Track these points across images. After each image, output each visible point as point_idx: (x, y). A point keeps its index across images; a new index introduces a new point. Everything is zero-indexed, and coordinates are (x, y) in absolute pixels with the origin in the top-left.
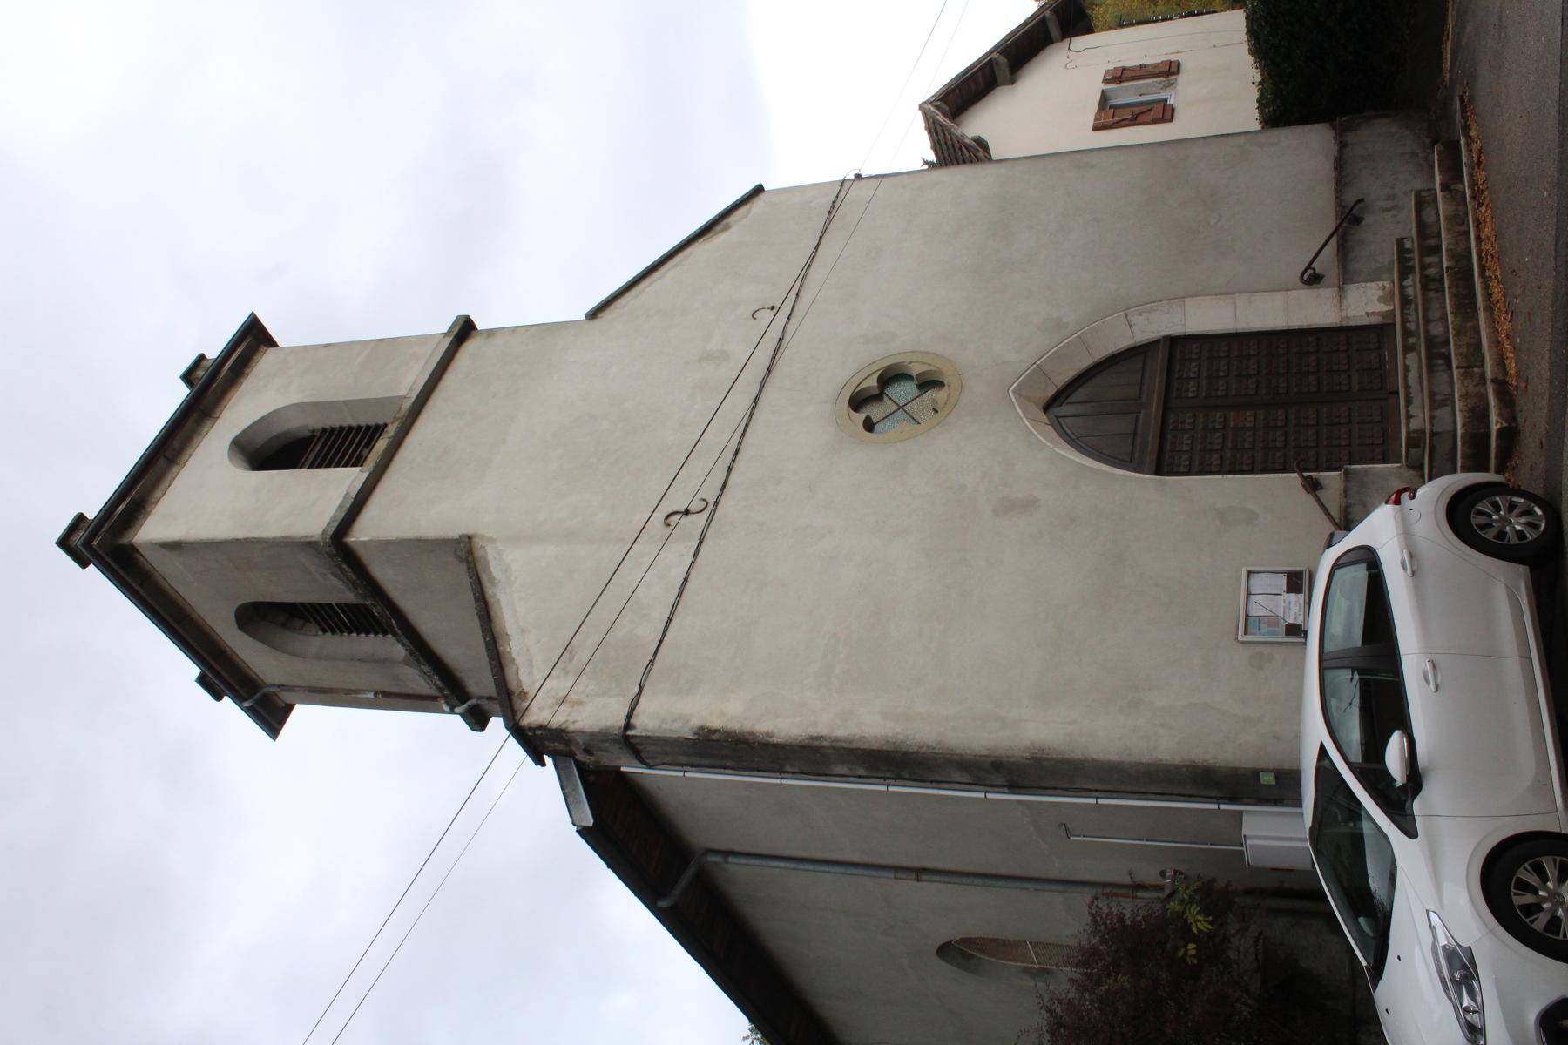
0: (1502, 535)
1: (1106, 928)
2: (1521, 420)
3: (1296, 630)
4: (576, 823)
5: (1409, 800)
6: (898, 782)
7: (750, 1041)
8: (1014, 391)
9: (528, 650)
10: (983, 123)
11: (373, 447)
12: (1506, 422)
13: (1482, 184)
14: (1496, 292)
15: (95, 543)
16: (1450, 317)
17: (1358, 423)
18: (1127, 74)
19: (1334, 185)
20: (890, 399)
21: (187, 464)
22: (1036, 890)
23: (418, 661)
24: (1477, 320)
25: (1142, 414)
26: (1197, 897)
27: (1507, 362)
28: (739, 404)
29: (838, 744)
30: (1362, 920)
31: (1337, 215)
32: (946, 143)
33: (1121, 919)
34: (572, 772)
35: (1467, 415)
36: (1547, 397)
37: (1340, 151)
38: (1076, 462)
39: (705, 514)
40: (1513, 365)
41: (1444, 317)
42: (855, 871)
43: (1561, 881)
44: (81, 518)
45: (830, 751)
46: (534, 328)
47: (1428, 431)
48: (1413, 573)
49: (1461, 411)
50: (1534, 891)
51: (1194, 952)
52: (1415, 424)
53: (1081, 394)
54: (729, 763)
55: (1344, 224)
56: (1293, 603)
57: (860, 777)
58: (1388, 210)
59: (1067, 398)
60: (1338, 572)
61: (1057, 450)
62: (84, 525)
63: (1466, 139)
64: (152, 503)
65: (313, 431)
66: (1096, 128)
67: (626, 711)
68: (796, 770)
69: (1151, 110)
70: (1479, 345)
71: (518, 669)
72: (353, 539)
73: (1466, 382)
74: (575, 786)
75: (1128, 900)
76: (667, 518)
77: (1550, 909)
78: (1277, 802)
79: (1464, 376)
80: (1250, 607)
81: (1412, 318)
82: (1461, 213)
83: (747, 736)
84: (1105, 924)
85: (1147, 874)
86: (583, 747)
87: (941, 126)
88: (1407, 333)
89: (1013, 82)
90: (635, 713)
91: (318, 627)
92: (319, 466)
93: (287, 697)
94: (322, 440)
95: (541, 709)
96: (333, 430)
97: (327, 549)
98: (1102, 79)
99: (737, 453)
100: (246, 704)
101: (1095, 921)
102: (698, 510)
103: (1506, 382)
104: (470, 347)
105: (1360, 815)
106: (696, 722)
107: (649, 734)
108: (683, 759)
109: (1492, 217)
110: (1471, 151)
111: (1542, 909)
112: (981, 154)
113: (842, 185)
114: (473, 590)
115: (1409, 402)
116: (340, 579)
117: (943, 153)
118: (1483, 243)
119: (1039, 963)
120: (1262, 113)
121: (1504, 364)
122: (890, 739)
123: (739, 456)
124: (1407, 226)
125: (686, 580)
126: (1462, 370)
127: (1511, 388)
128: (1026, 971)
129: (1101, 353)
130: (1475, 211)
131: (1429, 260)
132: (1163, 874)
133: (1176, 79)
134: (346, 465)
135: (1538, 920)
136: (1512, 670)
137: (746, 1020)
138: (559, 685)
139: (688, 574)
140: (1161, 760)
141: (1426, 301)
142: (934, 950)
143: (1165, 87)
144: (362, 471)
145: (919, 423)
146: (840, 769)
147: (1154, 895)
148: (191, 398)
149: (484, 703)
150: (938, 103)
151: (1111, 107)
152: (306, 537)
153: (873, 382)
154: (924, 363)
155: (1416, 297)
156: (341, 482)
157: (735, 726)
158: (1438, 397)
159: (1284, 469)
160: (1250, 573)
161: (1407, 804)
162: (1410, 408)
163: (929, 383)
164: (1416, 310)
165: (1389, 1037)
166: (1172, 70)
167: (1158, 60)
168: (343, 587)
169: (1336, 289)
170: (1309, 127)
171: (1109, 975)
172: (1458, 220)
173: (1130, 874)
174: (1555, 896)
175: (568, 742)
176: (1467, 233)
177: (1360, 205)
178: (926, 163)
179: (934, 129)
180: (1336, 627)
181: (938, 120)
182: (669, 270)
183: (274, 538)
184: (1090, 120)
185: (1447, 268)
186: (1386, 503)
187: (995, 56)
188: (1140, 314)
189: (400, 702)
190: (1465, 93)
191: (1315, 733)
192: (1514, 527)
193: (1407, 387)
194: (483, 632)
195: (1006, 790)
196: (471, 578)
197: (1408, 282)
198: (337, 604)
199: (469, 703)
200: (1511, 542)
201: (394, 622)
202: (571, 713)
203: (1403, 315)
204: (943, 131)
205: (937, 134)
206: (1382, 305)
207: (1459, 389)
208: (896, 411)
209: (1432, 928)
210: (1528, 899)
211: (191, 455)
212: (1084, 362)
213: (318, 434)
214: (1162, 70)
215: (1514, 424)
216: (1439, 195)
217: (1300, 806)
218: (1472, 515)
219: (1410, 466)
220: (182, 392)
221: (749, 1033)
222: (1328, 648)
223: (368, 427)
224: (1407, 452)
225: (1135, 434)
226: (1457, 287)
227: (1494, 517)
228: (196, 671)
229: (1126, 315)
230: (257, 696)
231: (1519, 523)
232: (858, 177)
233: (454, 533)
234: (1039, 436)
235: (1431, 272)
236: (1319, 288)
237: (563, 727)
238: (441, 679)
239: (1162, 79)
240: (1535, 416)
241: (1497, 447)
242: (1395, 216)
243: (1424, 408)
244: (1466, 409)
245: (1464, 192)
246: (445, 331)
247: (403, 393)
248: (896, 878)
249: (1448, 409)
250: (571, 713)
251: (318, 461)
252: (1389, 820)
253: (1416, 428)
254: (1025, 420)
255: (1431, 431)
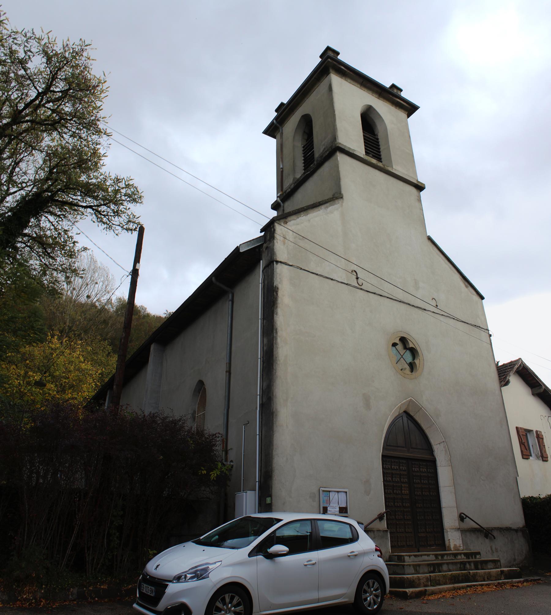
0: (366, 592)
1: (211, 440)
2: (411, 601)
3: (325, 511)
4: (241, 246)
5: (263, 554)
6: (262, 362)
7: (166, 312)
8: (411, 399)
9: (302, 223)
10: (515, 383)
11: (373, 158)
12: (410, 595)
13: (504, 587)
14: (461, 592)
15: (329, 60)
16: (450, 573)
17: (406, 536)
18: (541, 440)
19: (500, 527)
20: (405, 353)
21: (361, 90)
22: (224, 413)
23: (295, 183)
24: (449, 584)
25: (405, 449)
26: (223, 474)
27: (433, 596)
28: (400, 295)
29: (275, 339)
30: (217, 537)
31: (488, 528)
32: (506, 369)
33: (214, 445)
34: (259, 243)
35: (412, 579)
36: (421, 611)
37: (514, 530)
38: (385, 424)
39: (357, 285)
40: (432, 598)
41: (450, 571)
42: (228, 348)
43: (235, 612)
44: (338, 54)
45: (272, 336)
46: (423, 217)
47: (404, 563)
48: (349, 556)
49: (413, 577)
50: (230, 603)
51: (203, 473)
52: (407, 558)
53: (412, 425)
54: (265, 299)
55: (484, 531)
56: (335, 510)
57: (263, 348)
58: (491, 549)
59: (410, 420)
60: (348, 526)
61: (390, 416)
62: (335, 55)
63: (523, 581)
64: (345, 79)
65: (377, 135)
66: (517, 428)
67: (283, 261)
68: (264, 324)
69: (526, 450)
70: (440, 585)
71: (295, 220)
72: (338, 154)
73: (424, 579)
74: (254, 244)
75: (221, 448)
76: (355, 271)
77: (224, 608)
78: (260, 504)
79: (427, 578)
80: (333, 492)
81: (449, 558)
82: (492, 578)
83: (276, 306)
84: (212, 439)
85: (232, 455)
86: (268, 246)
87: (513, 367)
88: (442, 556)
89: (533, 394)
90: (282, 264)
91: (305, 144)
92: (364, 139)
93: (278, 136)
94: (373, 139)
95: (281, 230)
96: (378, 142)
97: (334, 145)
98: (537, 430)
99: (381, 296)
100: (275, 121)
101: (213, 435)
102: (358, 282)
103: (425, 595)
104: (414, 190)
105: (256, 536)
106: (280, 286)
107: (275, 270)
108: (266, 282)
109: (491, 591)
110: (518, 583)
111: (224, 605)
112: (503, 383)
113: (487, 330)
114: (323, 201)
115: (415, 556)
116: (323, 151)
117: (502, 368)
118: (480, 587)
119: (197, 416)
120: (527, 498)
121: (433, 595)
122: (277, 358)
123: (380, 296)
124: (484, 557)
125: (332, 279)
126: (429, 577)
127: (423, 597)
128: (195, 412)
129: (427, 432)
130: (494, 584)
131: (472, 565)
132: (232, 461)
133: (540, 460)
134: (365, 149)
135: (219, 603)
136: (314, 595)
137: (174, 311)
138: (290, 236)
139: (334, 280)
140: (274, 459)
141: (456, 563)
142: (201, 379)
143: (536, 456)
144: (363, 155)
145: (396, 363)
146: (265, 340)
147: (224, 458)
148: (386, 89)
149: (282, 209)
150: (522, 365)
151: (526, 434)
152: (338, 137)
153: (411, 345)
154: (420, 364)
155: (457, 559)
156: (360, 149)
157: (279, 301)
158: (418, 568)
159: (387, 506)
160: (346, 492)
161: (261, 553)
162: (413, 556)
163: (412, 366)
164: (452, 560)
165: (174, 548)
166: (544, 458)
167: (548, 453)
168: (320, 153)
169: (459, 528)
170: (523, 516)
171: (193, 441)
172: (489, 577)
173: (231, 449)
174: (229, 610)
175: (270, 240)
176: (484, 581)
177: (493, 537)
178: (498, 363)
179: (511, 365)
180: (327, 525)
181: (515, 366)
182: (449, 266)
183: (336, 125)
184: (520, 426)
185: (470, 572)
186: (376, 546)
187: (543, 387)
188: (444, 447)
189: (280, 177)
190: (542, 581)
191: (286, 518)
192: (368, 597)
193: (421, 555)
194: (308, 206)
195: (261, 402)
196: (327, 199)
197: (462, 555)
198: (313, 151)
199: (281, 203)
200: (363, 596)
201: (309, 172)
202: (280, 241)
203: (450, 554)
204: (511, 368)
205: (509, 366)
206: (453, 546)
207: (421, 576)
208: (401, 355)
209: (215, 563)
210: (228, 600)
211: (364, 91)
212: (424, 426)
213: (376, 137)
214: (544, 454)
215: (409, 598)
216: (499, 570)
217: (258, 513)
218: (373, 580)
219: (390, 556)
220: (388, 85)
221: (169, 312)
222: (319, 522)
223: (380, 155)
224: (396, 555)
225: (398, 447)
226: (462, 576)
227: (372, 589)
228: (285, 102)
229: (444, 442)
230: (278, 125)
231: (370, 599)
232: (490, 336)
233: (343, 192)
234: (395, 409)
235: (468, 566)
236: (458, 520)
237: (275, 238)
238: (289, 192)
239: (540, 454)
240: (412, 606)
241: (400, 591)
242: (489, 552)
243: (413, 562)
244: (414, 579)
245: (501, 580)
246: (419, 180)
247: (394, 167)
248: (227, 363)
249: (413, 572)
250: (280, 241)
251: (366, 138)
252: (254, 546)
253: (405, 559)
254: (400, 404)
255: (405, 565)
